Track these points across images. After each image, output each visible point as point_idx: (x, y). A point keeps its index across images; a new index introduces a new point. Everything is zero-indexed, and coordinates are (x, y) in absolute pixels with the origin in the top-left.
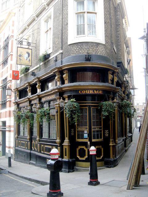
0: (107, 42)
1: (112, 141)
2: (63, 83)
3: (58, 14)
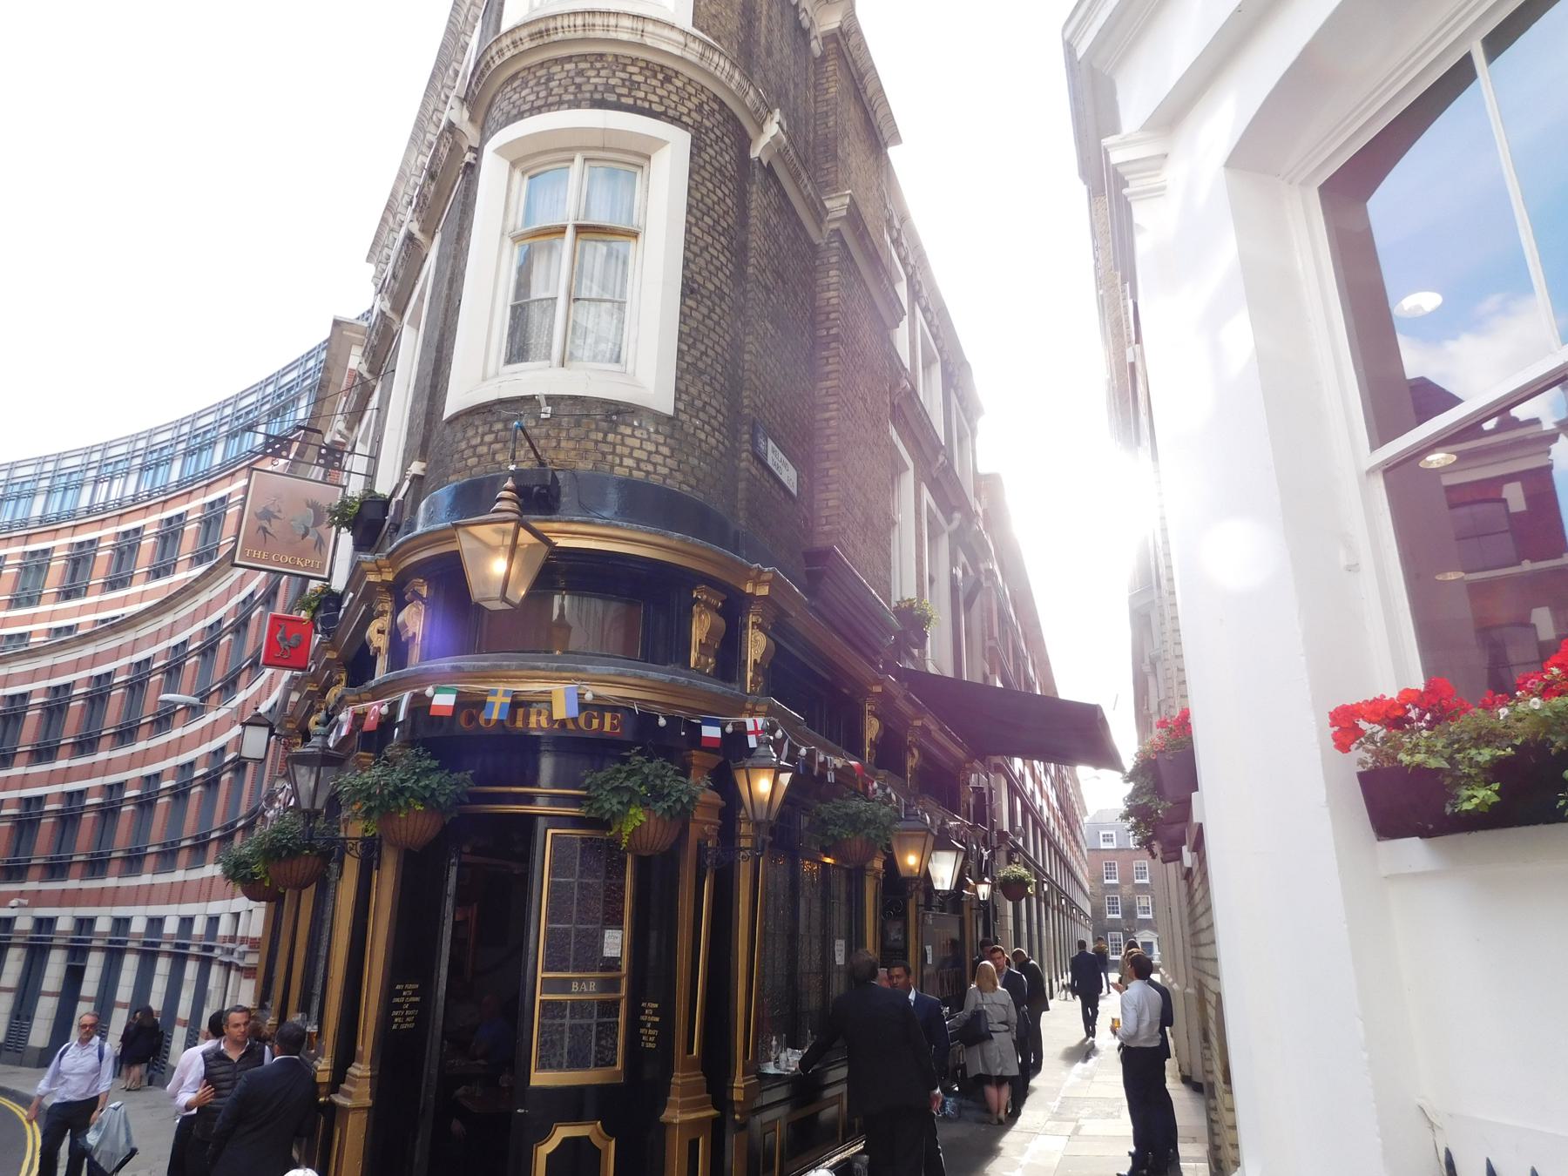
0: (698, 403)
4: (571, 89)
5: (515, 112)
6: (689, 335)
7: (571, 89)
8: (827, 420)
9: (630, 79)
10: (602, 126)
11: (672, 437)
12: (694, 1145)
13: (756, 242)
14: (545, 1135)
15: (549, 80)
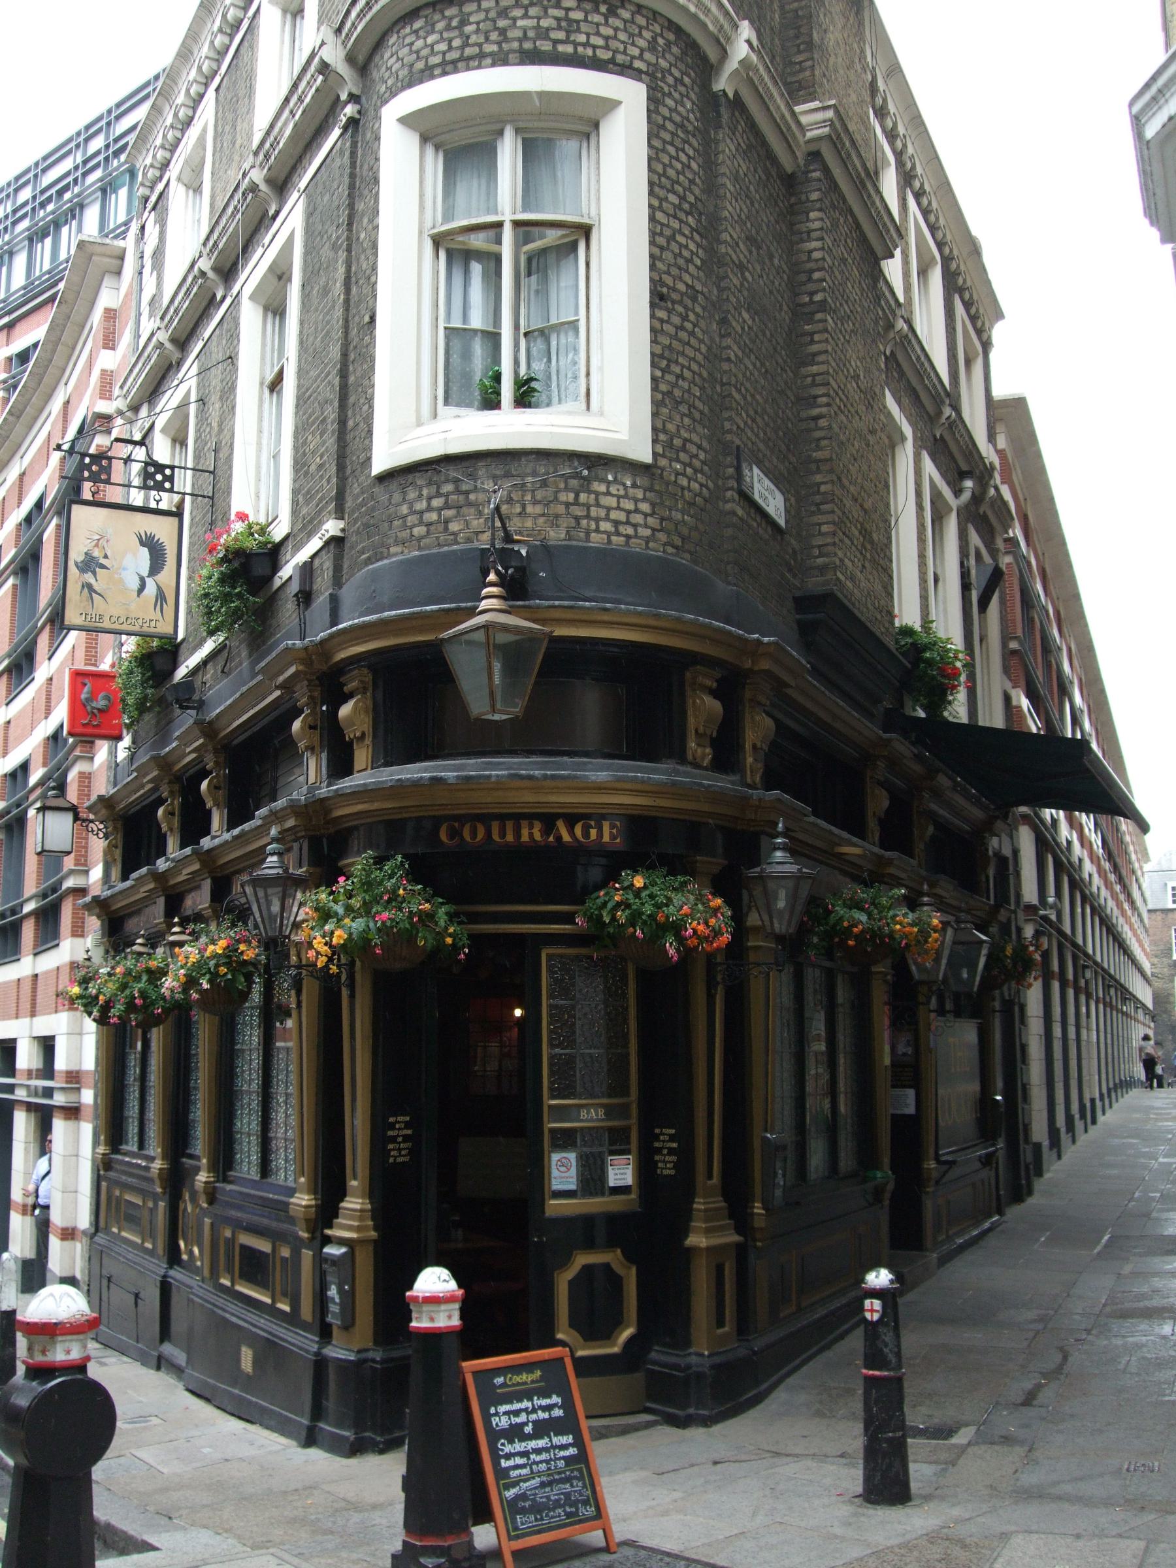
0: (677, 442)
1: (709, 1215)
2: (341, 765)
3: (326, 252)
4: (494, 36)
5: (420, 65)
6: (662, 356)
7: (494, 36)
8: (816, 418)
9: (567, 19)
10: (539, 89)
11: (651, 489)
12: (720, 1269)
13: (730, 209)
14: (565, 1262)
15: (463, 23)
